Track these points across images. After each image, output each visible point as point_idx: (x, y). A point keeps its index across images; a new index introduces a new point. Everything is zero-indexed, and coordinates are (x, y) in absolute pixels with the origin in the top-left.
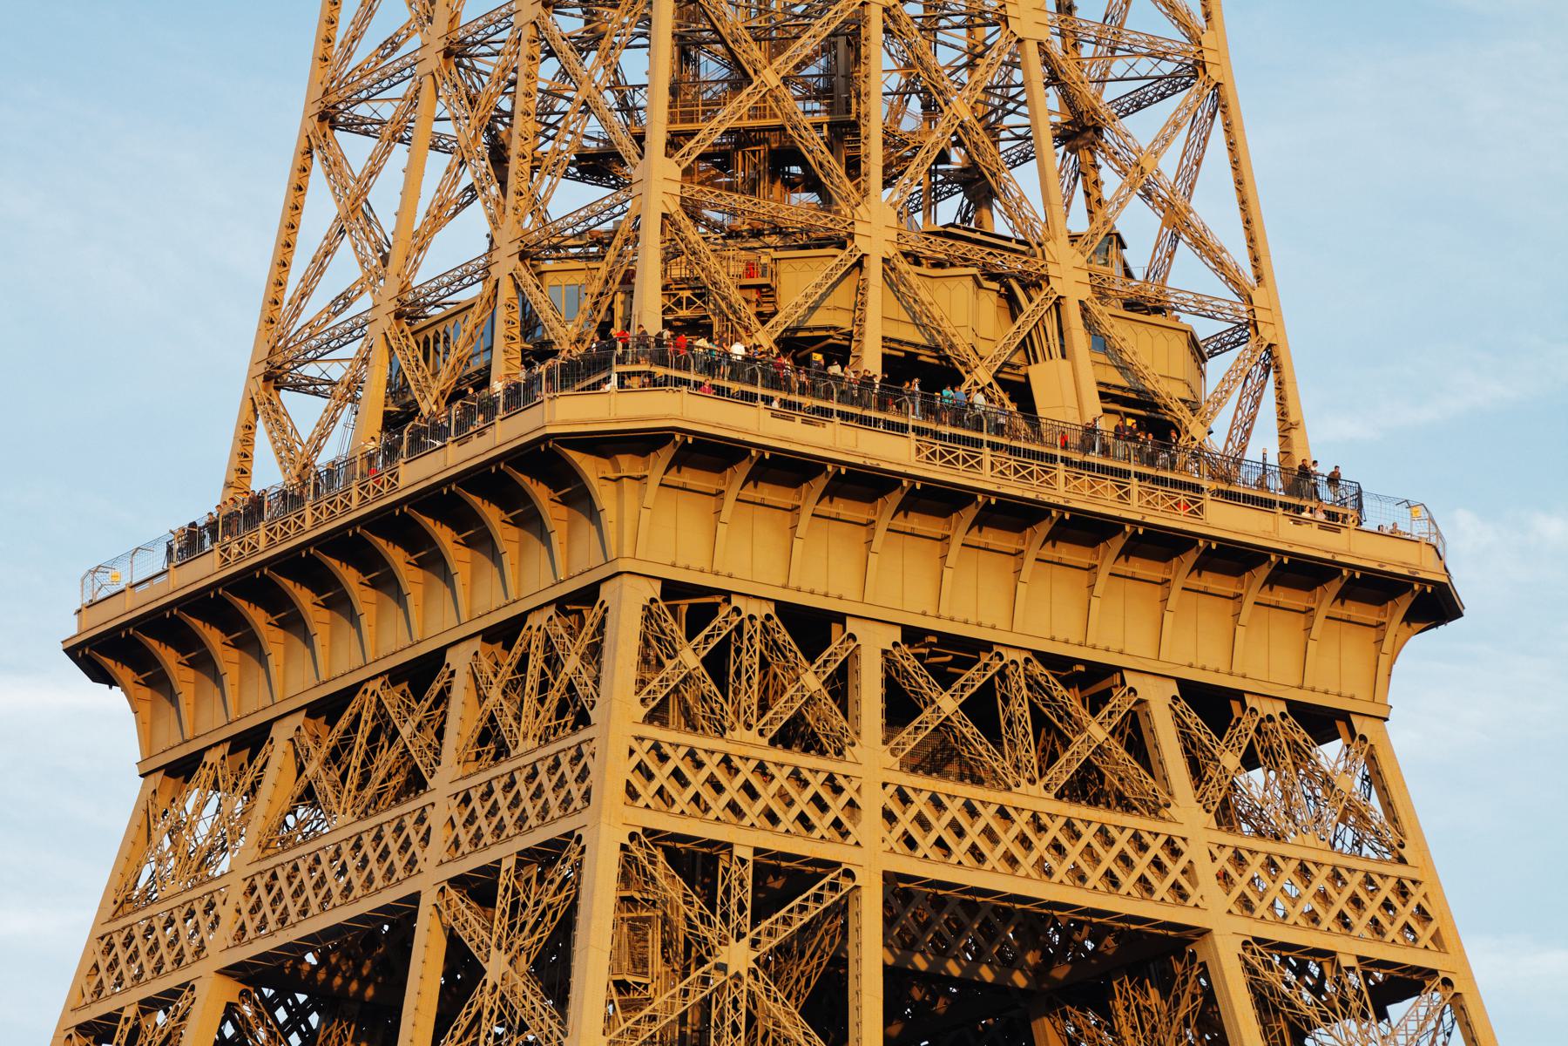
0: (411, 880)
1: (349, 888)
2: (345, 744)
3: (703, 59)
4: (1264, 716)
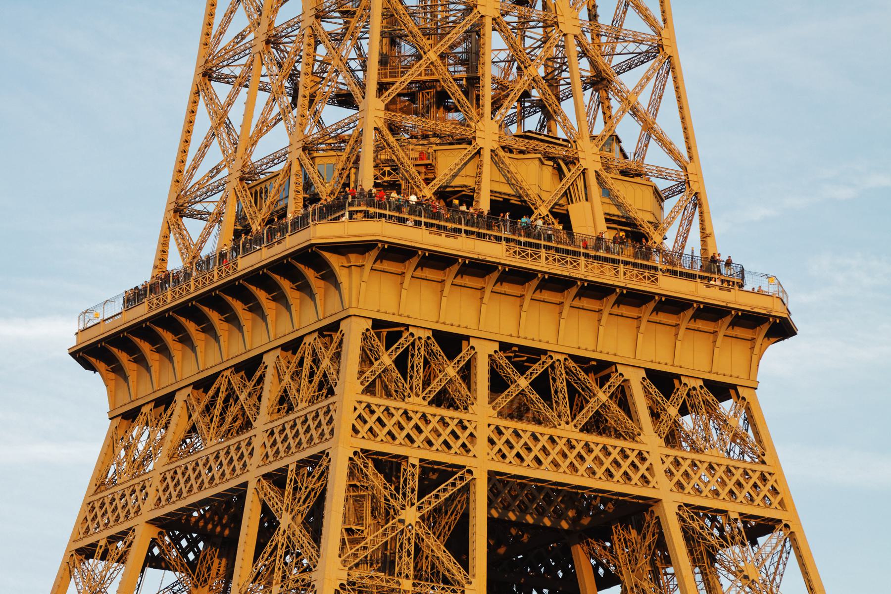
0: (264, 467)
2: (212, 404)
3: (403, 43)
4: (691, 388)
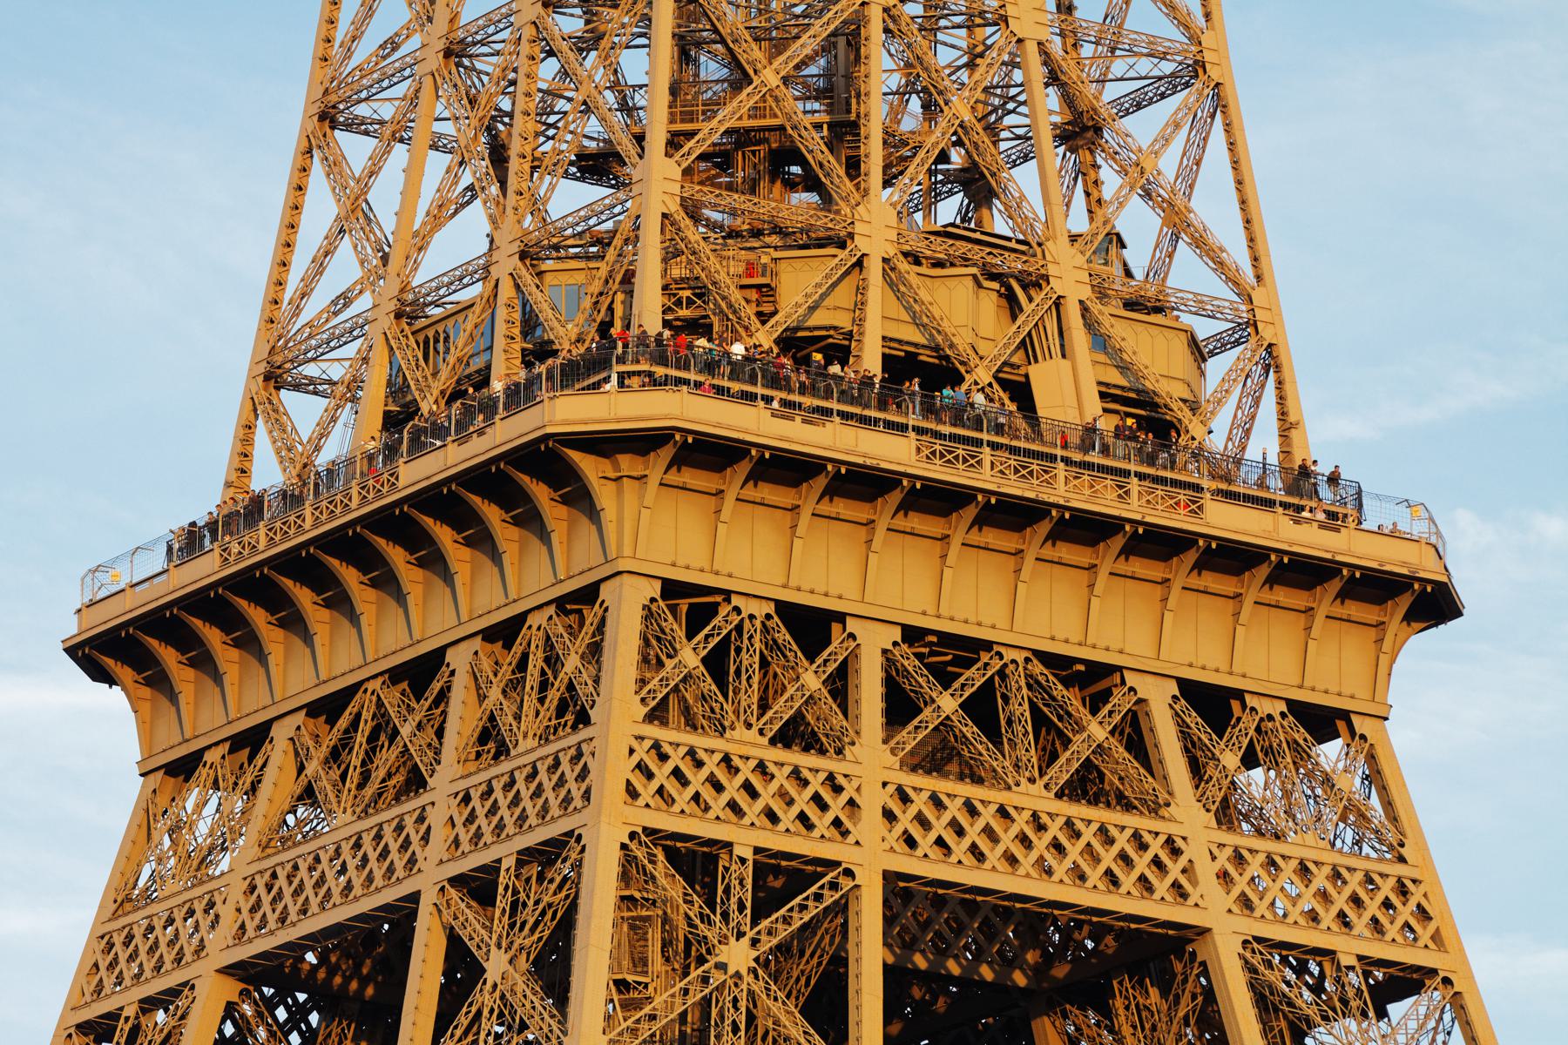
1: (349, 887)
2: (345, 743)
3: (703, 59)
4: (1264, 716)
